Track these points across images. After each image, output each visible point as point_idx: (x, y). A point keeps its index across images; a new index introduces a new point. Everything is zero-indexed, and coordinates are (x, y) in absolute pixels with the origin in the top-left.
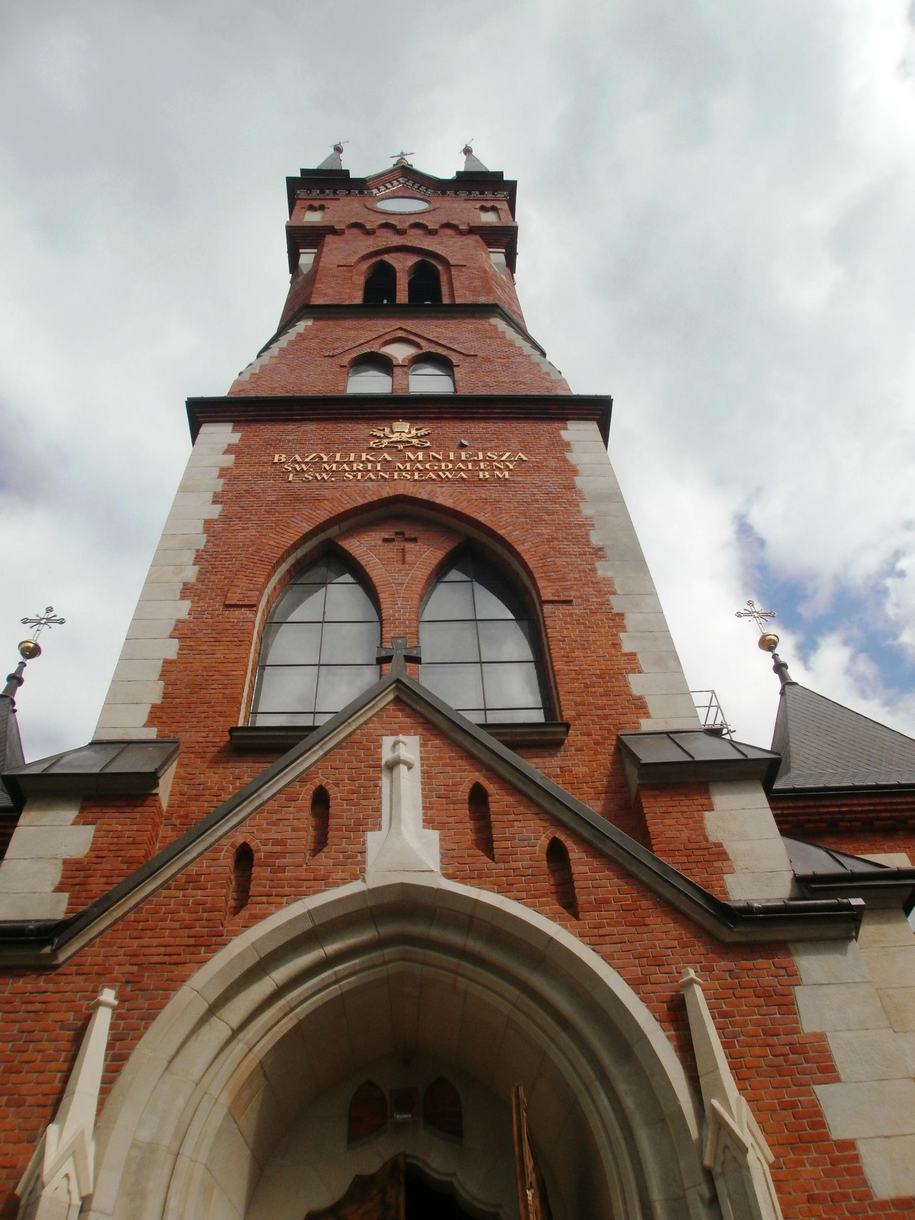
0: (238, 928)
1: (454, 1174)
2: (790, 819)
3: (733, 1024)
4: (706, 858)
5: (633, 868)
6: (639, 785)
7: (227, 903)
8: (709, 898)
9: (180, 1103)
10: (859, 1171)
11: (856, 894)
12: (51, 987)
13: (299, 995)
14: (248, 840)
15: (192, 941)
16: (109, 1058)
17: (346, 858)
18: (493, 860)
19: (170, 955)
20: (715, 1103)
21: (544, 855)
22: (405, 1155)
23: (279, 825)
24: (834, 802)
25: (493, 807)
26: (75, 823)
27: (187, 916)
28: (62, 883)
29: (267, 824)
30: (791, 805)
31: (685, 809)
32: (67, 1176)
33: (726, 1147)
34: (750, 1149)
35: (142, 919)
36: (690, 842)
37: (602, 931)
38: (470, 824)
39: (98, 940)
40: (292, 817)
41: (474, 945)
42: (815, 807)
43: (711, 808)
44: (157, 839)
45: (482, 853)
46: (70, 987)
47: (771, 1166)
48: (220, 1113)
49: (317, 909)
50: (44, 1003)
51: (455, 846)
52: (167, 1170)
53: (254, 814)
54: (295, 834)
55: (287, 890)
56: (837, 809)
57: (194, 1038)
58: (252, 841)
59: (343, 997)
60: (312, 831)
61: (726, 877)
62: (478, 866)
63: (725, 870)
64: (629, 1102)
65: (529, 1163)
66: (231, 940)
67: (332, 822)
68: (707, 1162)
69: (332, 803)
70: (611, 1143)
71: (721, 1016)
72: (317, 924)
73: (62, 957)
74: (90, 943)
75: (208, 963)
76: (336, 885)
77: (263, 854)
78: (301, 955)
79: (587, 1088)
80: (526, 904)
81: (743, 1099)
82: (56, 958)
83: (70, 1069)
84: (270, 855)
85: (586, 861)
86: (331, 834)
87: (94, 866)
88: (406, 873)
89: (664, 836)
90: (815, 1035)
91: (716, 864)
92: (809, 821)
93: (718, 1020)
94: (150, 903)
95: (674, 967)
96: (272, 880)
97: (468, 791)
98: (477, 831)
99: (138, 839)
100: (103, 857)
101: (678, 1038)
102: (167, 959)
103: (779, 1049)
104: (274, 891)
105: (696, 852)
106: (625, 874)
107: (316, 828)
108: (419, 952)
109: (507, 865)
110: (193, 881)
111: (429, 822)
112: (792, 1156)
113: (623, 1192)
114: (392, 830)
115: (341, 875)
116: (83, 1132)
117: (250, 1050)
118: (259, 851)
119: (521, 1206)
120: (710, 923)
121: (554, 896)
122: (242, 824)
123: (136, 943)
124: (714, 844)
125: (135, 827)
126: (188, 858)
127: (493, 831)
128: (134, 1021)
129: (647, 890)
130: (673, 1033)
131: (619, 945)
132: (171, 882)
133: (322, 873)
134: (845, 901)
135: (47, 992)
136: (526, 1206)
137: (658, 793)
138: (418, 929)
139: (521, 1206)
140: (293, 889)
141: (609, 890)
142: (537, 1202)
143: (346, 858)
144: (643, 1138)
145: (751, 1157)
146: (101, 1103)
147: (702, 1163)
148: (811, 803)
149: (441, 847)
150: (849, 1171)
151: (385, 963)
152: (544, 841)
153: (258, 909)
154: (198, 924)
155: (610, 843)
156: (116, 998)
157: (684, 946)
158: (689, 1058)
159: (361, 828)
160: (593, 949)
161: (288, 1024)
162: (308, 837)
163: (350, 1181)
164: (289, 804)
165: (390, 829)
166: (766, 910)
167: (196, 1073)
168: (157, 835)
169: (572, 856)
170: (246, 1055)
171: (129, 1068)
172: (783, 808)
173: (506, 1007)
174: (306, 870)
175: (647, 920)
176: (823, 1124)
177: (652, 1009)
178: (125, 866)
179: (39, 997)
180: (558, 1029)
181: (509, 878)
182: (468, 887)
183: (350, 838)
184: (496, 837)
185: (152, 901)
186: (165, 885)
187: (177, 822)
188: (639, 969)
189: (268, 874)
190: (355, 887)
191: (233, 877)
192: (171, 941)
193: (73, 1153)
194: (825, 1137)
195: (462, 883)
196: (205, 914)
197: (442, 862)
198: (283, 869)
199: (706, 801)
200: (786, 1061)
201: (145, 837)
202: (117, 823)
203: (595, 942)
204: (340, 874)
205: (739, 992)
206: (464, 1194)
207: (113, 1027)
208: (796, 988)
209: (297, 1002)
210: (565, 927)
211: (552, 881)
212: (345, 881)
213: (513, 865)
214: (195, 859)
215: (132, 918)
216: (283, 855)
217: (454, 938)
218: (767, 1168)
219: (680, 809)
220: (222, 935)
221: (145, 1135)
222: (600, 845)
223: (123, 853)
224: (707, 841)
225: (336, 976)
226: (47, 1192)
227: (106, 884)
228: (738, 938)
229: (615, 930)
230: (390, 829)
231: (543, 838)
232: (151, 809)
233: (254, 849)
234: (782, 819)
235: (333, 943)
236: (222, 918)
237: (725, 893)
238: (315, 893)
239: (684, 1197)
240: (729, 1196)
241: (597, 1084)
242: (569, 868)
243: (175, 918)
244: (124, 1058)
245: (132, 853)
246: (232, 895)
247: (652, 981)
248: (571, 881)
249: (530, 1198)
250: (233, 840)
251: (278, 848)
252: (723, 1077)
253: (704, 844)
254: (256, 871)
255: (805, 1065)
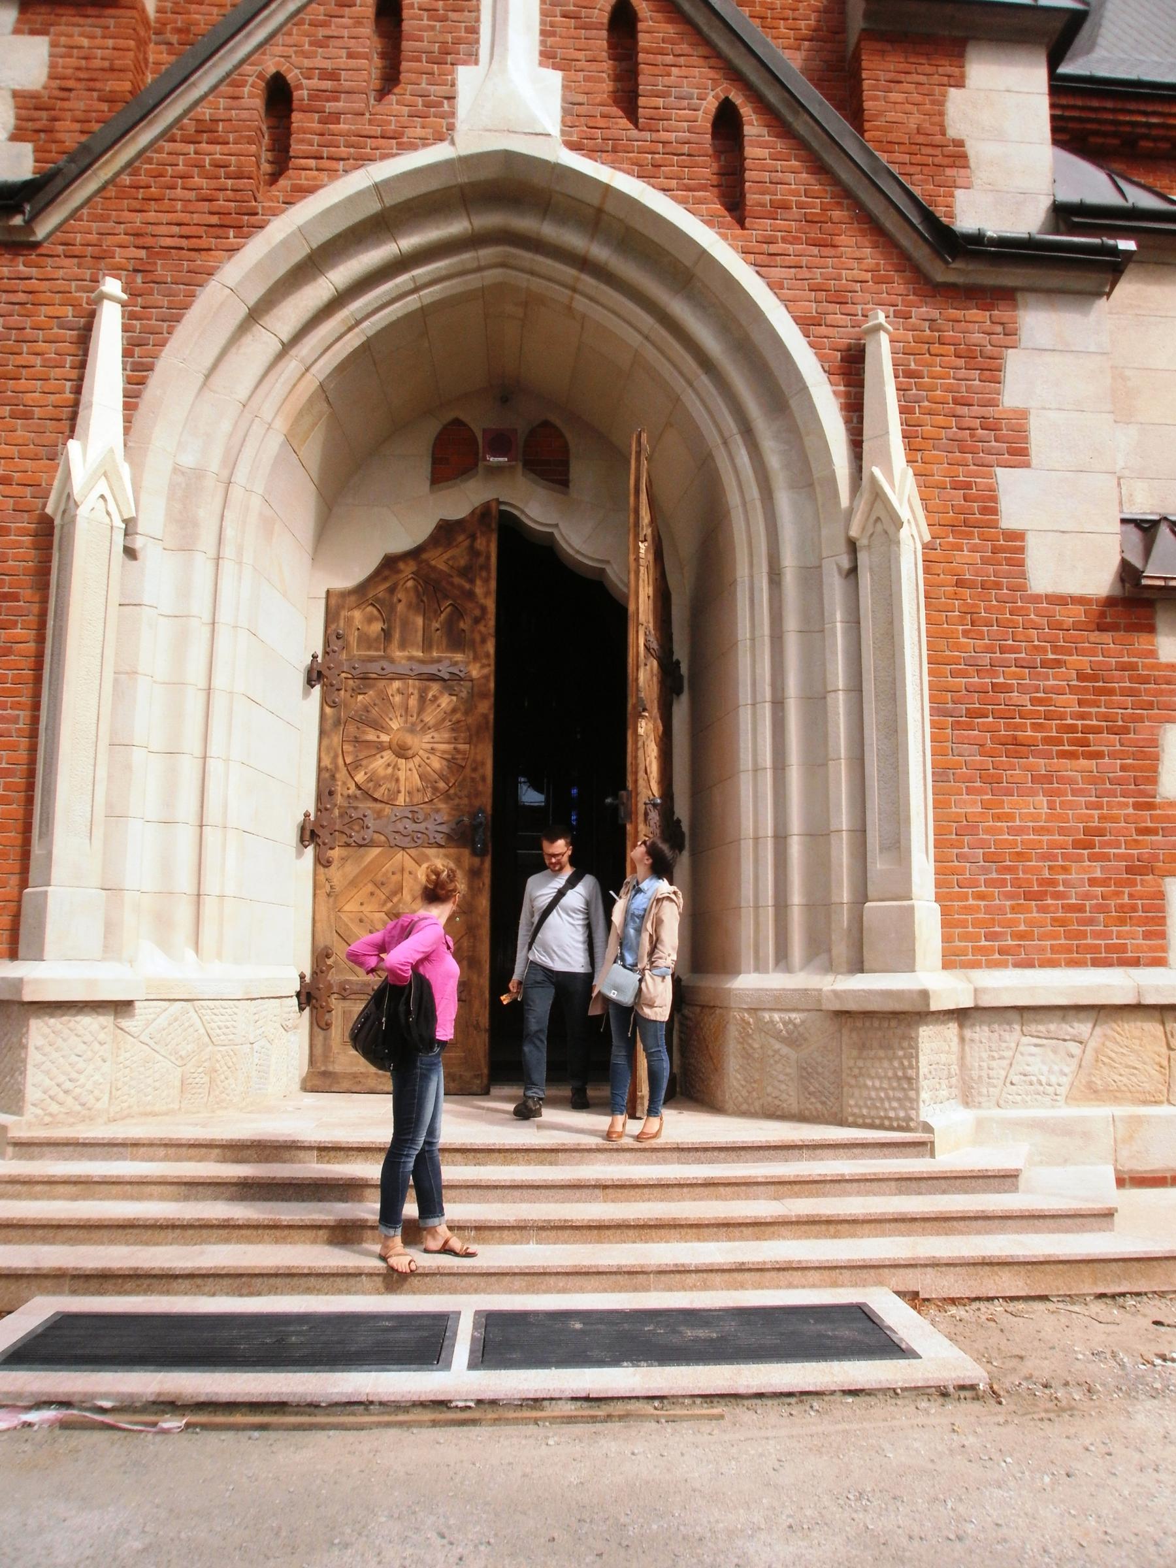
0: (276, 204)
1: (556, 526)
2: (1071, 125)
3: (919, 387)
4: (937, 160)
5: (831, 159)
6: (864, 30)
7: (259, 167)
8: (929, 217)
9: (226, 426)
10: (1021, 564)
11: (1126, 233)
12: (34, 271)
13: (366, 305)
14: (283, 70)
15: (214, 220)
16: (128, 368)
17: (428, 105)
18: (635, 121)
19: (187, 237)
20: (877, 471)
21: (709, 125)
22: (499, 503)
23: (328, 47)
24: (1143, 107)
25: (644, 40)
26: (17, 31)
27: (204, 183)
28: (17, 128)
29: (311, 44)
30: (1079, 103)
31: (923, 79)
32: (102, 497)
33: (878, 519)
34: (906, 524)
35: (142, 184)
36: (918, 133)
37: (773, 249)
38: (607, 65)
39: (85, 211)
40: (346, 35)
41: (600, 252)
42: (1114, 111)
43: (960, 84)
44: (147, 66)
45: (620, 113)
46: (60, 273)
47: (925, 546)
48: (275, 442)
49: (386, 182)
50: (31, 292)
51: (582, 98)
52: (218, 500)
53: (289, 25)
54: (353, 63)
55: (343, 151)
56: (1144, 119)
57: (234, 350)
58: (290, 70)
59: (424, 312)
60: (377, 61)
61: (959, 193)
62: (614, 133)
63: (959, 182)
64: (774, 462)
65: (645, 517)
66: (268, 222)
67: (406, 45)
68: (854, 532)
69: (406, 13)
70: (744, 504)
71: (906, 375)
72: (387, 205)
73: (42, 231)
74: (74, 214)
75: (242, 251)
76: (413, 147)
77: (305, 92)
78: (367, 250)
79: (725, 443)
80: (675, 199)
81: (910, 472)
82: (33, 233)
83: (81, 378)
84: (316, 95)
85: (767, 142)
86: (405, 65)
87: (59, 104)
88: (512, 135)
89: (883, 119)
90: (1015, 411)
91: (948, 171)
92: (1096, 133)
93: (901, 379)
94: (149, 161)
95: (859, 307)
96: (322, 135)
97: (609, 8)
98: (617, 78)
99: (118, 63)
100: (70, 90)
101: (847, 395)
102: (184, 243)
103: (968, 422)
104: (325, 152)
105: (925, 150)
106: (819, 168)
107: (383, 56)
108: (526, 257)
109: (655, 136)
110: (206, 130)
111: (548, 57)
112: (951, 539)
113: (751, 555)
114: (495, 66)
115: (419, 132)
116: (112, 451)
117: (307, 370)
118: (300, 87)
119: (632, 557)
120: (921, 253)
121: (715, 190)
122: (272, 42)
123: (138, 218)
124: (954, 141)
125: (110, 43)
126: (196, 93)
127: (642, 79)
128: (153, 322)
129: (845, 194)
130: (842, 388)
131: (793, 270)
132: (175, 131)
133: (393, 127)
134: (1111, 242)
135: (30, 279)
136: (637, 559)
137: (889, 47)
138: (525, 223)
139: (632, 557)
140: (352, 150)
141: (791, 190)
142: (651, 557)
143: (428, 105)
144: (784, 501)
145: (904, 533)
146: (128, 420)
147: (847, 533)
148: (1109, 104)
149: (564, 100)
150: (1010, 562)
151: (479, 269)
152: (710, 104)
153: (303, 179)
154: (221, 195)
155: (807, 117)
156: (124, 291)
157: (878, 281)
158: (855, 420)
159: (449, 58)
160: (757, 272)
161: (353, 341)
162: (370, 69)
163: (433, 526)
164: (340, 11)
165: (491, 63)
166: (1003, 242)
167: (242, 392)
168: (146, 60)
169: (748, 130)
170: (303, 375)
171: (155, 380)
172: (1063, 107)
173: (634, 339)
174: (370, 121)
175: (839, 240)
176: (995, 511)
177: (821, 358)
178: (105, 107)
179: (21, 285)
180: (699, 371)
181: (657, 156)
182: (598, 165)
183: (432, 74)
184: (644, 90)
185: (152, 158)
186: (166, 135)
187: (174, 39)
188: (814, 305)
189: (316, 126)
190: (438, 153)
191: (264, 128)
192: (185, 217)
193: (105, 474)
194: (994, 525)
195: (590, 158)
196: (230, 182)
197: (564, 123)
198: (335, 117)
199: (955, 71)
200: (972, 436)
201: (128, 60)
202: (82, 35)
203: (762, 262)
204: (419, 130)
205: (936, 348)
206: (565, 546)
207: (126, 329)
208: (1010, 351)
209: (364, 313)
210: (724, 237)
211: (715, 167)
212: (425, 142)
213: (663, 136)
214: (206, 95)
215: (128, 183)
216: (335, 95)
217: (574, 240)
218: (919, 547)
219: (916, 78)
220: (256, 214)
221: (188, 460)
222: (790, 118)
223: (98, 85)
224: (944, 134)
225: (415, 282)
226: (82, 513)
227: (82, 132)
228: (951, 278)
229: (790, 248)
230: (491, 63)
231: (710, 98)
232: (129, 13)
233: (292, 83)
234: (1062, 124)
235: (411, 234)
236: (254, 188)
237: (951, 216)
238: (384, 157)
239: (820, 567)
240: (871, 570)
241: (738, 439)
242: (741, 148)
243: (188, 186)
244: (142, 382)
245: (112, 85)
246: (265, 155)
247: (829, 323)
248: (742, 170)
249: (642, 551)
250: (259, 68)
251: (328, 85)
252: (892, 443)
253: (938, 139)
254: (296, 116)
255: (993, 443)
